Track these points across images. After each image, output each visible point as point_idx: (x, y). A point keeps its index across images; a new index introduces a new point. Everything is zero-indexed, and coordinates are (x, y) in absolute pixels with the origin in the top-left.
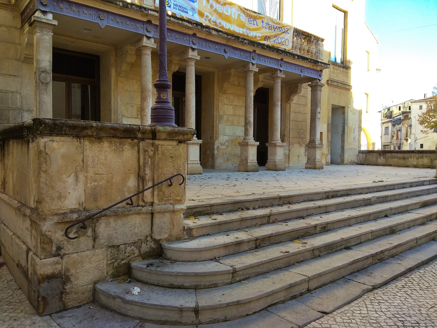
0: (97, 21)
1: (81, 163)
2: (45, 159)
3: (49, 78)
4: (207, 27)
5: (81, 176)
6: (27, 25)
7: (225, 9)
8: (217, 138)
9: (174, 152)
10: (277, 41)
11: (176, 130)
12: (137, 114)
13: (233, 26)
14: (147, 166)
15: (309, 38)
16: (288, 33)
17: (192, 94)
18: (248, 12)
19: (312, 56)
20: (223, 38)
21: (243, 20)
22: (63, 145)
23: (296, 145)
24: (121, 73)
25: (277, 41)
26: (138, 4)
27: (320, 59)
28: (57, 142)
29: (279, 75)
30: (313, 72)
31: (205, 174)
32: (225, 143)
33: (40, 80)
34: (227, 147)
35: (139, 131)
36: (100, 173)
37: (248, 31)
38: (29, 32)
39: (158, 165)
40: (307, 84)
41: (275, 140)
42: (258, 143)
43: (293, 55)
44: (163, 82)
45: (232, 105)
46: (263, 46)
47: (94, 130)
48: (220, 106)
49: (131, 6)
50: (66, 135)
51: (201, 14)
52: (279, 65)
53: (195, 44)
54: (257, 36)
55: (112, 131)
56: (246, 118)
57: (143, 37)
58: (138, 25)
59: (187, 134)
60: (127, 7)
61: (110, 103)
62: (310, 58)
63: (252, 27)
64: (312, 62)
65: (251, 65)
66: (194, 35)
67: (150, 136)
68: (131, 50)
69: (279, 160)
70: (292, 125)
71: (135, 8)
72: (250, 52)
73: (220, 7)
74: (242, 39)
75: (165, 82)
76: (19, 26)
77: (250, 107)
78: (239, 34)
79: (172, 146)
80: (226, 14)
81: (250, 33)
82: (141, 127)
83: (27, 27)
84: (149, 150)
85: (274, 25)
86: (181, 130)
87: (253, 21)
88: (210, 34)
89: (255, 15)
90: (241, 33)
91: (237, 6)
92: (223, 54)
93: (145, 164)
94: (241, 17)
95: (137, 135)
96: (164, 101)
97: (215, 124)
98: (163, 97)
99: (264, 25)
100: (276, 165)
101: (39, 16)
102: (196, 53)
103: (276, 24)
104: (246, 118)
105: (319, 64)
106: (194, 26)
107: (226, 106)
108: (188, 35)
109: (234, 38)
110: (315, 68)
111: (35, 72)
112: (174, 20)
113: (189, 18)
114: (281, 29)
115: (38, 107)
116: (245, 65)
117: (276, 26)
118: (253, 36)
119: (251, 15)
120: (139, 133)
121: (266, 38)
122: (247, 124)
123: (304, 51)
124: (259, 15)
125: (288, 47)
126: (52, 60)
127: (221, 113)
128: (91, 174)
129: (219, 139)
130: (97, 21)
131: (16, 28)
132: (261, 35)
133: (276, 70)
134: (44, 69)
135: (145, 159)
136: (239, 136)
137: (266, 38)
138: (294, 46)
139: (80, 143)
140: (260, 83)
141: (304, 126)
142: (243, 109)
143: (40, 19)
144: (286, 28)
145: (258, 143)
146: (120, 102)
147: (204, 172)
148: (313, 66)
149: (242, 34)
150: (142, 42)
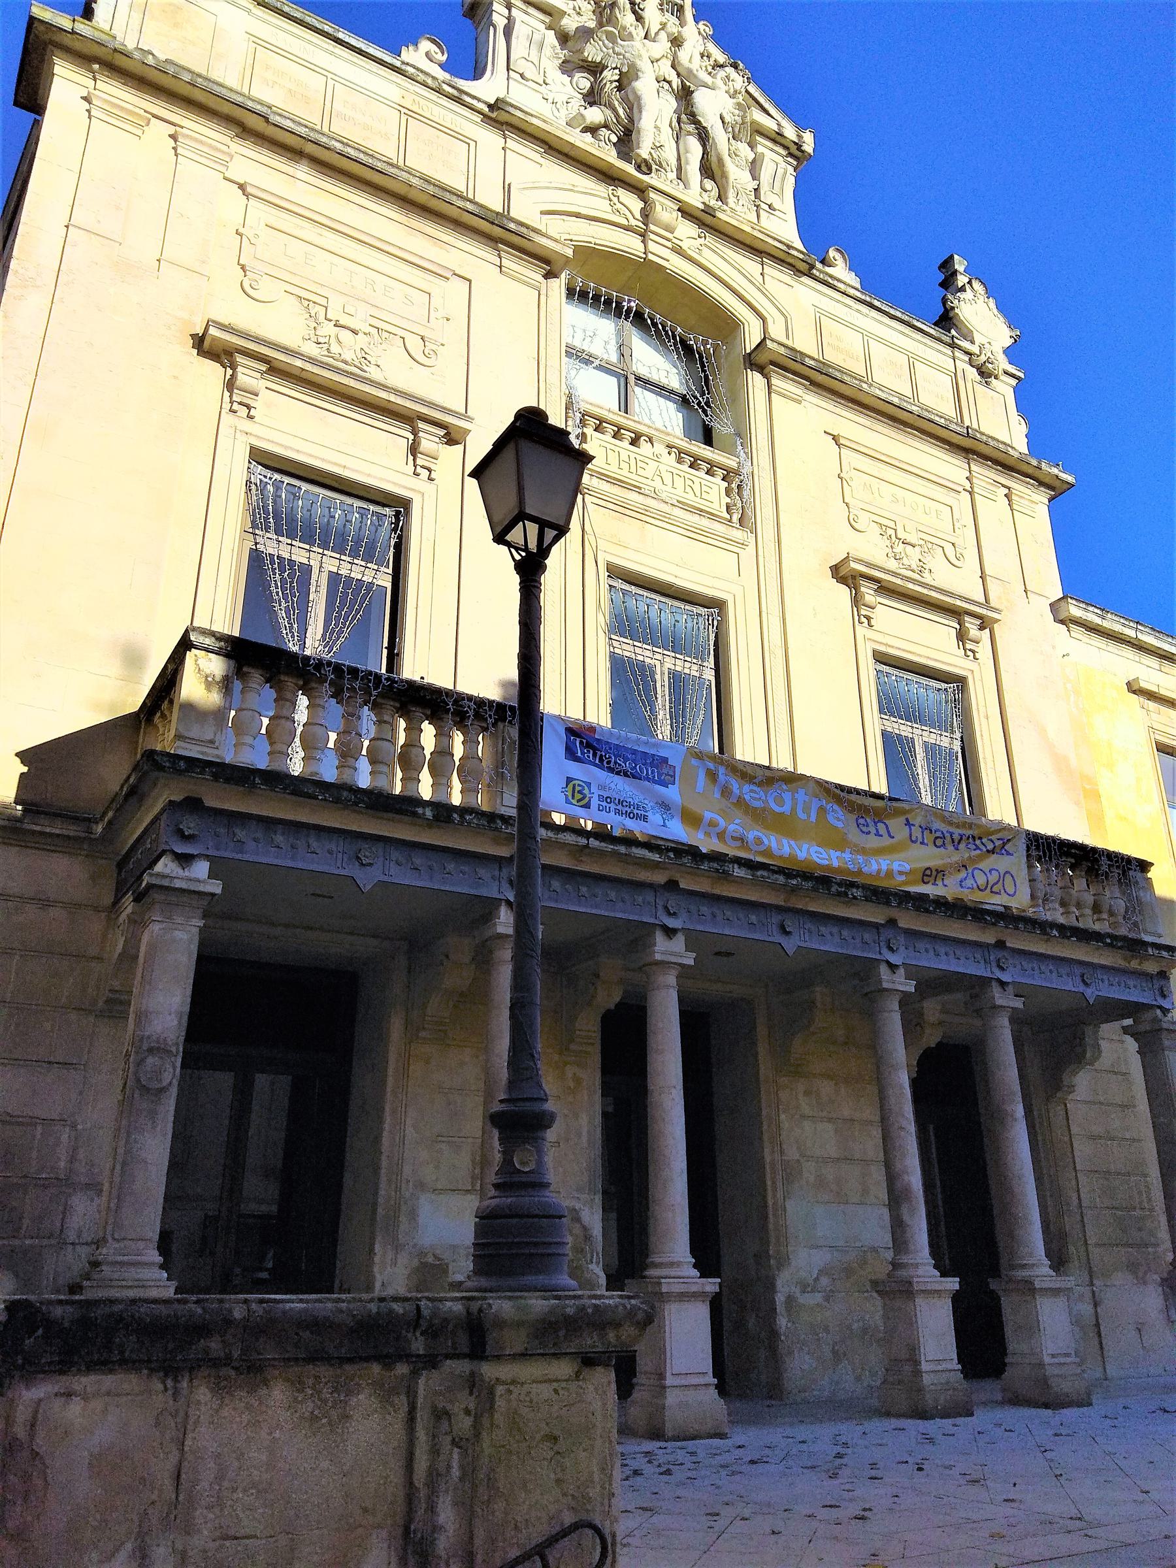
0: (352, 870)
1: (168, 1484)
2: (26, 1478)
3: (171, 1070)
4: (716, 857)
5: (161, 1550)
6: (129, 897)
7: (773, 796)
8: (784, 1261)
9: (564, 1412)
10: (970, 882)
11: (568, 1310)
12: (472, 1177)
13: (805, 847)
14: (443, 1487)
15: (1093, 865)
16: (1008, 853)
17: (674, 1091)
18: (853, 797)
19: (1114, 925)
20: (773, 887)
21: (840, 825)
22: (105, 1411)
23: (1121, 1278)
24: (424, 1028)
25: (970, 882)
26: (485, 808)
27: (1146, 932)
28: (86, 1399)
29: (999, 1002)
30: (1131, 983)
31: (740, 1436)
32: (817, 1279)
33: (138, 1080)
34: (827, 1299)
35: (417, 1325)
36: (242, 1532)
37: (859, 857)
38: (131, 920)
39: (491, 1482)
40: (1116, 1025)
41: (1024, 1266)
42: (953, 1284)
43: (1042, 927)
44: (522, 1104)
45: (830, 1120)
46: (920, 903)
47: (234, 1336)
48: (786, 1125)
49: (462, 816)
50: (127, 1364)
51: (691, 819)
52: (994, 964)
53: (675, 914)
54: (895, 872)
55: (306, 1335)
56: (892, 1178)
57: (498, 907)
58: (482, 872)
59: (617, 1325)
60: (448, 820)
61: (377, 1140)
62: (1110, 931)
63: (872, 842)
64: (1119, 948)
65: (884, 970)
66: (672, 885)
67: (463, 1342)
68: (460, 948)
69: (1053, 1356)
70: (1089, 1190)
71: (475, 821)
72: (876, 926)
73: (755, 792)
74: (840, 884)
75: (528, 1104)
76: (108, 900)
77: (902, 1128)
78: (828, 868)
79: (555, 1385)
80: (777, 809)
81: (867, 862)
82: (428, 1307)
83: (128, 905)
84: (456, 1408)
85: (952, 829)
86: (590, 1311)
87: (876, 823)
88: (725, 879)
89: (879, 804)
90: (835, 864)
91: (812, 784)
92: (778, 938)
93: (434, 1476)
94: (831, 818)
95: (409, 1342)
96: (524, 1179)
97: (770, 1202)
98: (523, 1163)
99: (917, 832)
100: (1044, 1382)
101: (167, 871)
102: (679, 942)
103: (958, 827)
104: (892, 1178)
105: (1150, 950)
106: (669, 858)
107: (807, 1124)
108: (651, 886)
109: (810, 884)
110: (1134, 964)
111: (128, 1055)
112: (603, 844)
113: (654, 834)
114: (978, 842)
115: (117, 1179)
116: (864, 970)
117: (960, 835)
118: (879, 871)
119: (865, 806)
120: (418, 1334)
121: (929, 875)
122: (896, 1198)
123: (1079, 905)
124: (895, 804)
125: (1019, 899)
126: (187, 1009)
127: (792, 1154)
128: (202, 1539)
129: (794, 1263)
130: (352, 870)
131: (96, 909)
132: (907, 867)
133: (984, 982)
134: (158, 1042)
135: (435, 1451)
136: (874, 1250)
137: (930, 876)
138: (1040, 894)
139: (176, 1395)
140: (928, 1031)
141: (1140, 1193)
142: (877, 1133)
143: (168, 879)
144: (999, 835)
145: (953, 1284)
146: (410, 1131)
147: (736, 1419)
148: (1125, 959)
149: (839, 867)
150: (495, 924)
